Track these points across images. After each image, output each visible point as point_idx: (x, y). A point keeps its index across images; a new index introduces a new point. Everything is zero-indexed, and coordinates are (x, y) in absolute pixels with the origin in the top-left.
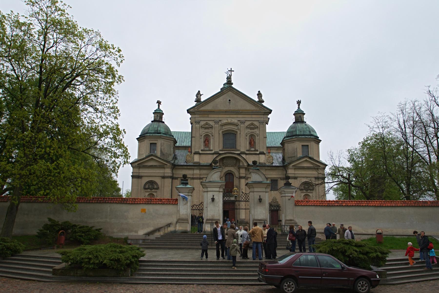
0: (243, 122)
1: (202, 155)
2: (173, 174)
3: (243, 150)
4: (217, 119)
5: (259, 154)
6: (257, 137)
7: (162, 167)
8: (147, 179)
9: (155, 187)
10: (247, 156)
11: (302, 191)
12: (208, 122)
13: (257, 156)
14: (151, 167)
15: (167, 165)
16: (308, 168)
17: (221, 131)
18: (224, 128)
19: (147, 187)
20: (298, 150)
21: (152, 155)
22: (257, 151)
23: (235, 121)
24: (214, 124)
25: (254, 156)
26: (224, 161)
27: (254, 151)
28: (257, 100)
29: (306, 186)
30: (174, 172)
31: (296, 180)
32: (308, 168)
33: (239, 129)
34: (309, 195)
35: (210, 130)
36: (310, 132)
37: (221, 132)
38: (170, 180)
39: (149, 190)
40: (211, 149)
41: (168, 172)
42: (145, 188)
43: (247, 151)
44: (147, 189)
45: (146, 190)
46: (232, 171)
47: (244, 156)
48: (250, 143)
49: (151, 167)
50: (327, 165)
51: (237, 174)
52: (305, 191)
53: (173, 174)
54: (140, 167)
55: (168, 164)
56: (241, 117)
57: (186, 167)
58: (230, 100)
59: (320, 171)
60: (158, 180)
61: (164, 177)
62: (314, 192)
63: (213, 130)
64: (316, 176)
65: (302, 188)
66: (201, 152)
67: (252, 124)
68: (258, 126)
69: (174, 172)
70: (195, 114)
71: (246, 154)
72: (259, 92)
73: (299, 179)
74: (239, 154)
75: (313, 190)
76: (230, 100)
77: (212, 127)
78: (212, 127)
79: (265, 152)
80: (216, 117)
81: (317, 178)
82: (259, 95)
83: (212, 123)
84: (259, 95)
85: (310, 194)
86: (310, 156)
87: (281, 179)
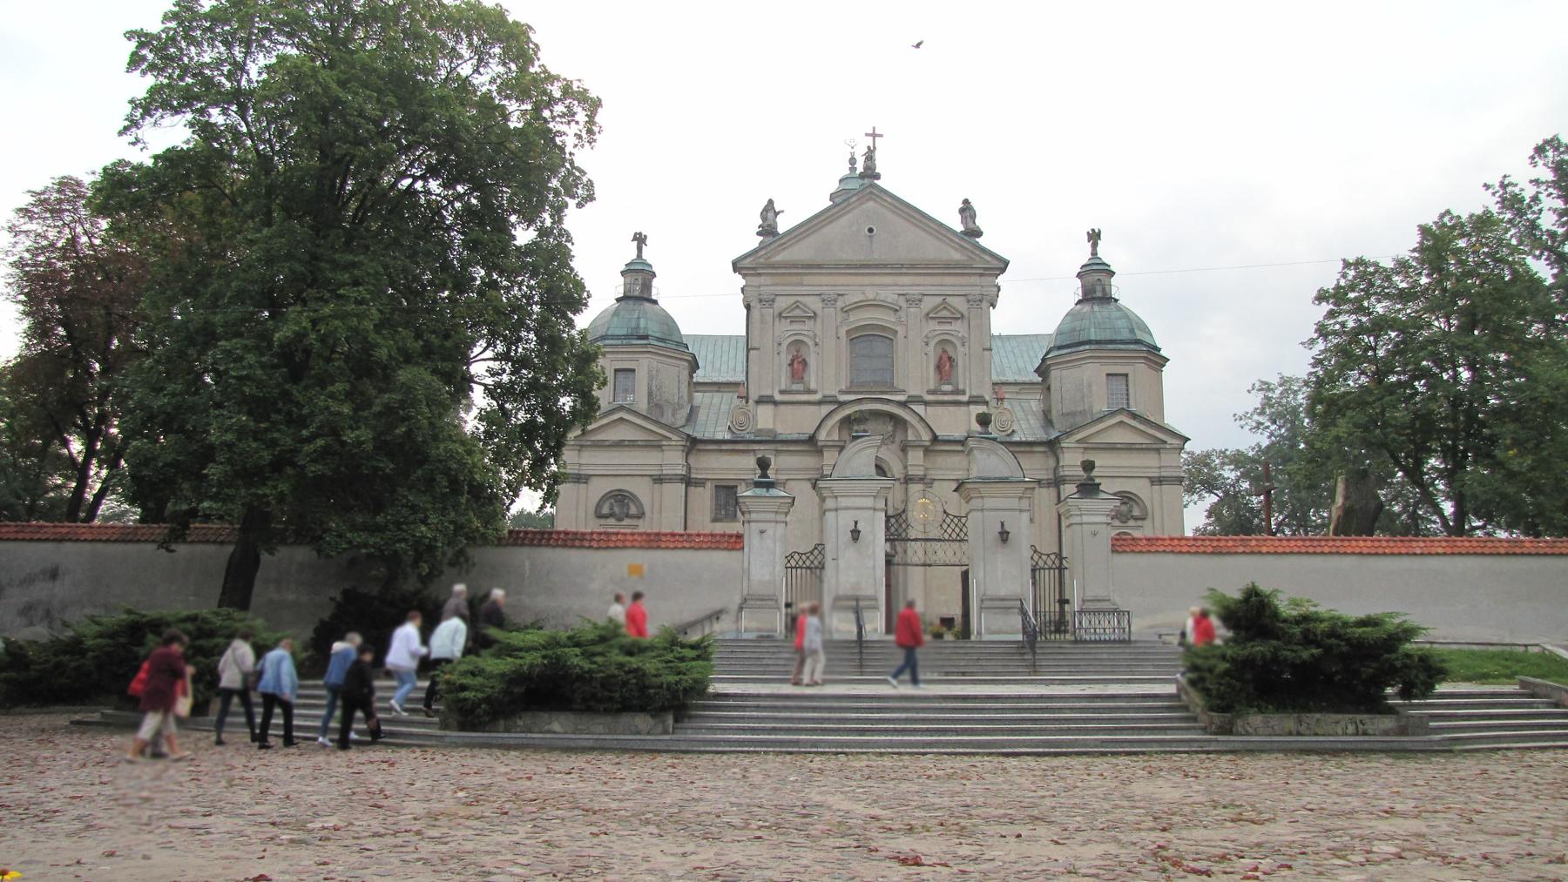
0: (914, 301)
2: (689, 469)
7: (654, 445)
9: (1136, 512)
13: (964, 409)
19: (605, 510)
22: (963, 393)
23: (888, 295)
25: (952, 409)
27: (952, 393)
28: (958, 227)
32: (1129, 448)
35: (809, 324)
36: (1132, 331)
41: (673, 461)
53: (689, 469)
55: (674, 438)
58: (871, 230)
61: (659, 480)
66: (778, 397)
71: (926, 403)
74: (903, 404)
76: (871, 230)
82: (967, 210)
84: (967, 210)
86: (1133, 409)
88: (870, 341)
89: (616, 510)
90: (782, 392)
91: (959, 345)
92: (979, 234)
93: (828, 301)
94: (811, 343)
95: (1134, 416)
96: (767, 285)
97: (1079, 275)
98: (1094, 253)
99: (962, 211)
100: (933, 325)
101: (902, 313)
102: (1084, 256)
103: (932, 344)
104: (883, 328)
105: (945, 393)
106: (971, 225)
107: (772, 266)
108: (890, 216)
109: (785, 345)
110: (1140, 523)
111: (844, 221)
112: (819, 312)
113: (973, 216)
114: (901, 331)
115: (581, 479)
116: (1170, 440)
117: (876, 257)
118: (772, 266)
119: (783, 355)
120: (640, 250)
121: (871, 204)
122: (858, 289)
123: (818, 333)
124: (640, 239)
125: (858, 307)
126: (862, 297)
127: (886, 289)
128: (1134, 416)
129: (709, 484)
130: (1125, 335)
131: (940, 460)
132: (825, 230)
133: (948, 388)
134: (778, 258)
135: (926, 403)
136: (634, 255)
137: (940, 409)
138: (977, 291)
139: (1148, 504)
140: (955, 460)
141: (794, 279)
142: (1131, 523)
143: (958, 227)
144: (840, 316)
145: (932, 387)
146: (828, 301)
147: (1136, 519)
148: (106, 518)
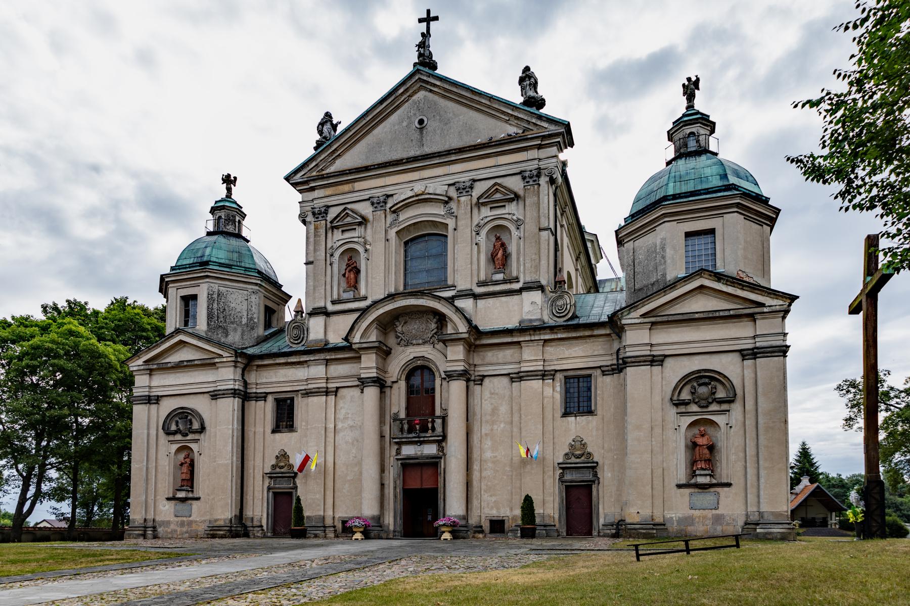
0: (465, 189)
1: (334, 319)
2: (246, 384)
3: (463, 283)
4: (465, 178)
5: (520, 291)
6: (515, 233)
7: (208, 364)
8: (167, 406)
9: (721, 394)
10: (481, 303)
11: (682, 409)
12: (498, 181)
13: (516, 298)
14: (180, 366)
15: (221, 356)
16: (711, 318)
17: (396, 229)
18: (402, 217)
19: (173, 427)
20: (669, 252)
21: (700, 272)
22: (517, 279)
23: (438, 187)
24: (371, 209)
25: (504, 299)
26: (399, 329)
27: (505, 281)
28: (516, 97)
29: (703, 390)
30: (252, 378)
31: (657, 369)
32: (711, 318)
33: (451, 214)
34: (713, 423)
35: (359, 231)
36: (724, 176)
37: (392, 233)
38: (237, 402)
39: (178, 437)
40: (363, 292)
41: (227, 376)
42: (168, 433)
43: (481, 284)
44: (685, 403)
45: (171, 438)
46: (428, 360)
47: (466, 304)
48: (493, 258)
49: (180, 366)
50: (793, 298)
51: (443, 366)
52: (694, 408)
53: (246, 384)
54: (151, 370)
55: (225, 354)
56: (461, 171)
57: (282, 360)
58: (421, 122)
59: (764, 326)
60: (201, 405)
61: (215, 395)
62: (736, 408)
63: (369, 230)
64: (748, 345)
65: (685, 395)
66: (331, 308)
67: (496, 188)
68: (521, 193)
69: (252, 378)
70: (313, 189)
71: (476, 297)
72: (527, 69)
73: (669, 362)
74: (451, 301)
75: (731, 401)
76: (421, 122)
77: (364, 222)
78: (364, 222)
79: (544, 282)
80: (374, 186)
81: (751, 354)
82: (527, 79)
83: (365, 209)
84: (527, 79)
85: (719, 419)
86: (720, 270)
87: (604, 373)
88: (423, 241)
89: (181, 427)
90: (334, 302)
91: (512, 228)
92: (541, 103)
93: (379, 203)
94: (360, 249)
95: (719, 277)
96: (328, 197)
97: (213, 210)
98: (690, 107)
99: (521, 80)
100: (486, 212)
101: (453, 205)
102: (680, 107)
103: (484, 232)
104: (434, 224)
105: (497, 283)
106: (531, 93)
107: (329, 176)
108: (442, 102)
109: (337, 255)
110: (725, 407)
111: (394, 118)
112: (370, 217)
113: (535, 85)
114: (451, 223)
115: (151, 400)
116: (768, 301)
117: (427, 150)
118: (322, 177)
119: (336, 266)
120: (229, 190)
121: (421, 94)
122: (402, 186)
123: (369, 238)
124: (229, 181)
125: (407, 204)
126: (411, 194)
127: (435, 180)
128: (719, 277)
129: (270, 398)
130: (716, 182)
131: (491, 356)
132: (376, 131)
133: (500, 277)
134: (332, 169)
135: (476, 297)
136: (223, 193)
137: (491, 301)
138: (533, 165)
139: (736, 382)
140: (508, 354)
141: (346, 188)
142: (714, 407)
143: (516, 97)
144: (390, 217)
145: (483, 277)
146: (379, 203)
147: (720, 402)
148: (896, 464)
